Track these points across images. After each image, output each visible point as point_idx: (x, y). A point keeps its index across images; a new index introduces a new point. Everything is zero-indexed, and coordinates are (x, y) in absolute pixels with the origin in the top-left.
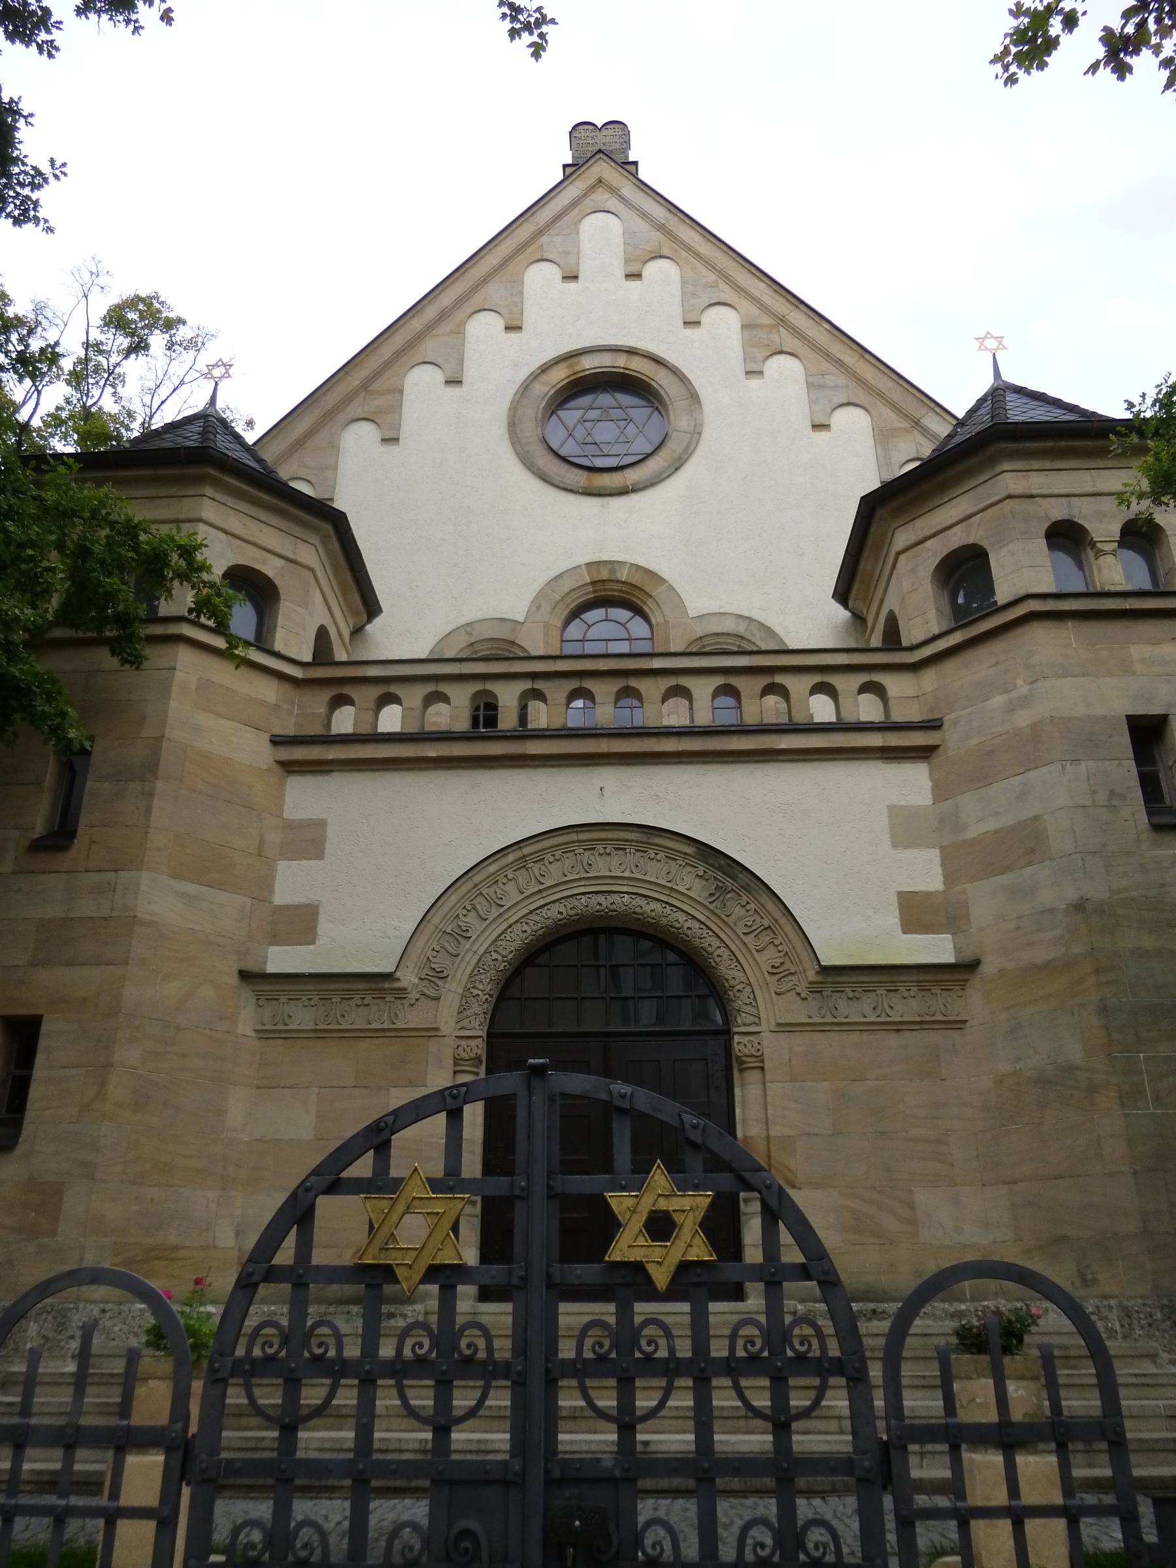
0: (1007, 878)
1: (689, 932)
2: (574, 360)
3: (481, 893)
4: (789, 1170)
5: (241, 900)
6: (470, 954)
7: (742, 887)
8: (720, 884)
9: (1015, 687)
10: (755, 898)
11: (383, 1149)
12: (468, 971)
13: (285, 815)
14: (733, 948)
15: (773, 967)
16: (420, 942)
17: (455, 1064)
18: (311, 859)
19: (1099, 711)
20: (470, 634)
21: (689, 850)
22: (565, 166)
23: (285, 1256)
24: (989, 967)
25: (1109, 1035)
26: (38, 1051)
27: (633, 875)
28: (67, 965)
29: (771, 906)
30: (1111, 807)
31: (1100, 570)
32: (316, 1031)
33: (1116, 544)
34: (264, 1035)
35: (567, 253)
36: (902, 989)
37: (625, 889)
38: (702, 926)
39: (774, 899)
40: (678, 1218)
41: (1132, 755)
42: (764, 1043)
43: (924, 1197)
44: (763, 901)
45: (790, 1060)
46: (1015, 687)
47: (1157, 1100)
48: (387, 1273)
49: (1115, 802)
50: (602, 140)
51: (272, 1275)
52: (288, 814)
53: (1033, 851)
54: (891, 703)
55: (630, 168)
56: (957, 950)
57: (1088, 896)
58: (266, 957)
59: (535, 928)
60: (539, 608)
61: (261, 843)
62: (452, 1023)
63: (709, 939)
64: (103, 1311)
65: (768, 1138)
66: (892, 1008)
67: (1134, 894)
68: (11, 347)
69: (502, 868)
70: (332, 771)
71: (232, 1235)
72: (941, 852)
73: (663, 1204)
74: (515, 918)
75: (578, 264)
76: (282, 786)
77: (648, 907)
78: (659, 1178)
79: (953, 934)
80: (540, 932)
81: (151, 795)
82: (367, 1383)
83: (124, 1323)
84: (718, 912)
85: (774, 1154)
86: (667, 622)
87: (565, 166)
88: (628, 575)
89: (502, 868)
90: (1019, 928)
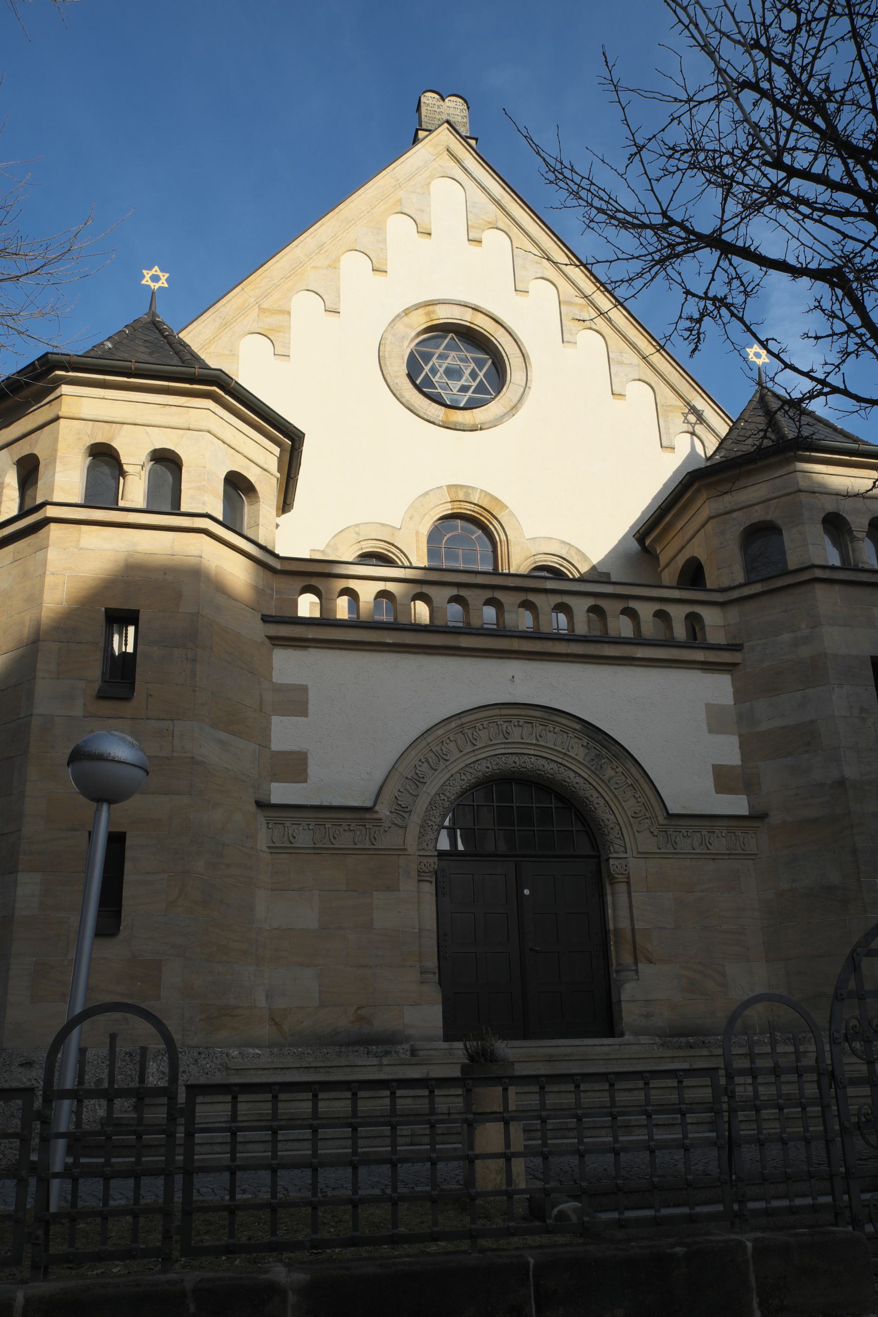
2: (431, 308)
3: (431, 750)
7: (613, 755)
8: (598, 753)
10: (623, 764)
13: (274, 680)
14: (607, 798)
15: (635, 813)
17: (419, 875)
18: (298, 716)
20: (358, 534)
21: (577, 727)
26: (126, 860)
27: (538, 743)
29: (633, 770)
32: (314, 848)
33: (865, 534)
34: (273, 849)
35: (422, 211)
36: (717, 831)
37: (532, 752)
38: (585, 782)
39: (636, 765)
41: (873, 684)
44: (628, 767)
45: (647, 877)
56: (751, 806)
58: (270, 791)
60: (411, 518)
63: (590, 791)
64: (200, 1053)
65: (633, 930)
66: (711, 844)
69: (446, 732)
70: (309, 647)
72: (740, 738)
74: (456, 769)
75: (430, 223)
77: (550, 767)
79: (747, 795)
80: (473, 781)
83: (212, 1062)
84: (597, 772)
88: (479, 498)
89: (446, 732)
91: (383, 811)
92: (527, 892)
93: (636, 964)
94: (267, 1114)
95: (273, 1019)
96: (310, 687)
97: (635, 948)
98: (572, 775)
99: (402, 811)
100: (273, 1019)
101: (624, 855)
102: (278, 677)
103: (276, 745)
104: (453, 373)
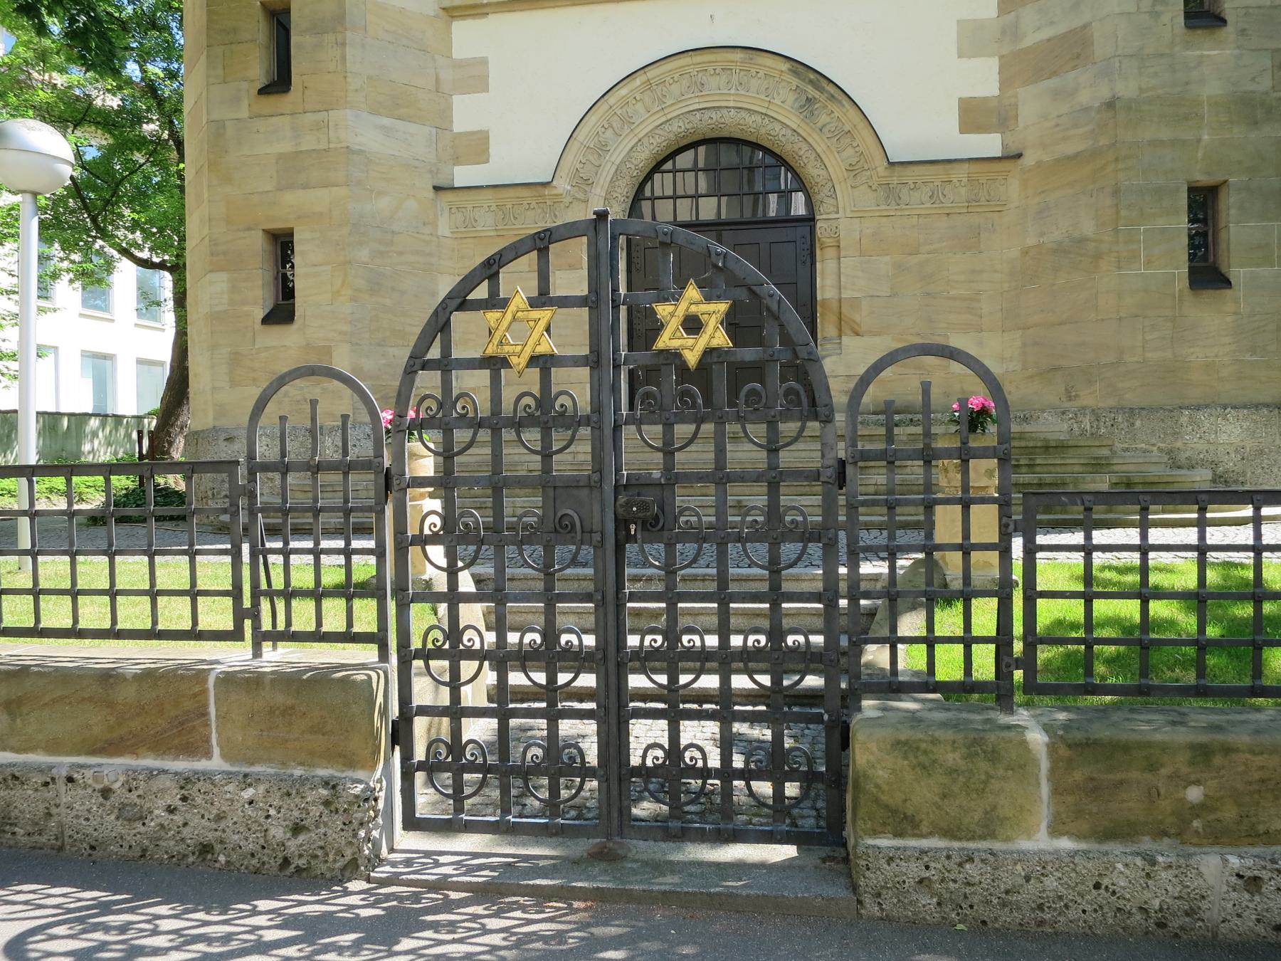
0: (1053, 82)
1: (783, 139)
4: (854, 322)
6: (609, 164)
11: (493, 277)
16: (569, 156)
23: (434, 353)
24: (1029, 160)
25: (1118, 213)
28: (304, 188)
37: (731, 104)
40: (704, 318)
42: (840, 227)
47: (1149, 263)
48: (503, 362)
51: (426, 366)
52: (457, 54)
53: (1078, 56)
57: (1120, 95)
59: (659, 141)
61: (437, 81)
65: (840, 300)
67: (1160, 92)
73: (693, 309)
74: (644, 133)
76: (449, 25)
77: (751, 120)
79: (1003, 133)
80: (665, 144)
81: (344, 44)
82: (496, 431)
85: (844, 310)
90: (1057, 125)
93: (840, 336)
96: (490, 59)
97: (840, 319)
98: (778, 127)
101: (836, 216)
103: (458, 127)
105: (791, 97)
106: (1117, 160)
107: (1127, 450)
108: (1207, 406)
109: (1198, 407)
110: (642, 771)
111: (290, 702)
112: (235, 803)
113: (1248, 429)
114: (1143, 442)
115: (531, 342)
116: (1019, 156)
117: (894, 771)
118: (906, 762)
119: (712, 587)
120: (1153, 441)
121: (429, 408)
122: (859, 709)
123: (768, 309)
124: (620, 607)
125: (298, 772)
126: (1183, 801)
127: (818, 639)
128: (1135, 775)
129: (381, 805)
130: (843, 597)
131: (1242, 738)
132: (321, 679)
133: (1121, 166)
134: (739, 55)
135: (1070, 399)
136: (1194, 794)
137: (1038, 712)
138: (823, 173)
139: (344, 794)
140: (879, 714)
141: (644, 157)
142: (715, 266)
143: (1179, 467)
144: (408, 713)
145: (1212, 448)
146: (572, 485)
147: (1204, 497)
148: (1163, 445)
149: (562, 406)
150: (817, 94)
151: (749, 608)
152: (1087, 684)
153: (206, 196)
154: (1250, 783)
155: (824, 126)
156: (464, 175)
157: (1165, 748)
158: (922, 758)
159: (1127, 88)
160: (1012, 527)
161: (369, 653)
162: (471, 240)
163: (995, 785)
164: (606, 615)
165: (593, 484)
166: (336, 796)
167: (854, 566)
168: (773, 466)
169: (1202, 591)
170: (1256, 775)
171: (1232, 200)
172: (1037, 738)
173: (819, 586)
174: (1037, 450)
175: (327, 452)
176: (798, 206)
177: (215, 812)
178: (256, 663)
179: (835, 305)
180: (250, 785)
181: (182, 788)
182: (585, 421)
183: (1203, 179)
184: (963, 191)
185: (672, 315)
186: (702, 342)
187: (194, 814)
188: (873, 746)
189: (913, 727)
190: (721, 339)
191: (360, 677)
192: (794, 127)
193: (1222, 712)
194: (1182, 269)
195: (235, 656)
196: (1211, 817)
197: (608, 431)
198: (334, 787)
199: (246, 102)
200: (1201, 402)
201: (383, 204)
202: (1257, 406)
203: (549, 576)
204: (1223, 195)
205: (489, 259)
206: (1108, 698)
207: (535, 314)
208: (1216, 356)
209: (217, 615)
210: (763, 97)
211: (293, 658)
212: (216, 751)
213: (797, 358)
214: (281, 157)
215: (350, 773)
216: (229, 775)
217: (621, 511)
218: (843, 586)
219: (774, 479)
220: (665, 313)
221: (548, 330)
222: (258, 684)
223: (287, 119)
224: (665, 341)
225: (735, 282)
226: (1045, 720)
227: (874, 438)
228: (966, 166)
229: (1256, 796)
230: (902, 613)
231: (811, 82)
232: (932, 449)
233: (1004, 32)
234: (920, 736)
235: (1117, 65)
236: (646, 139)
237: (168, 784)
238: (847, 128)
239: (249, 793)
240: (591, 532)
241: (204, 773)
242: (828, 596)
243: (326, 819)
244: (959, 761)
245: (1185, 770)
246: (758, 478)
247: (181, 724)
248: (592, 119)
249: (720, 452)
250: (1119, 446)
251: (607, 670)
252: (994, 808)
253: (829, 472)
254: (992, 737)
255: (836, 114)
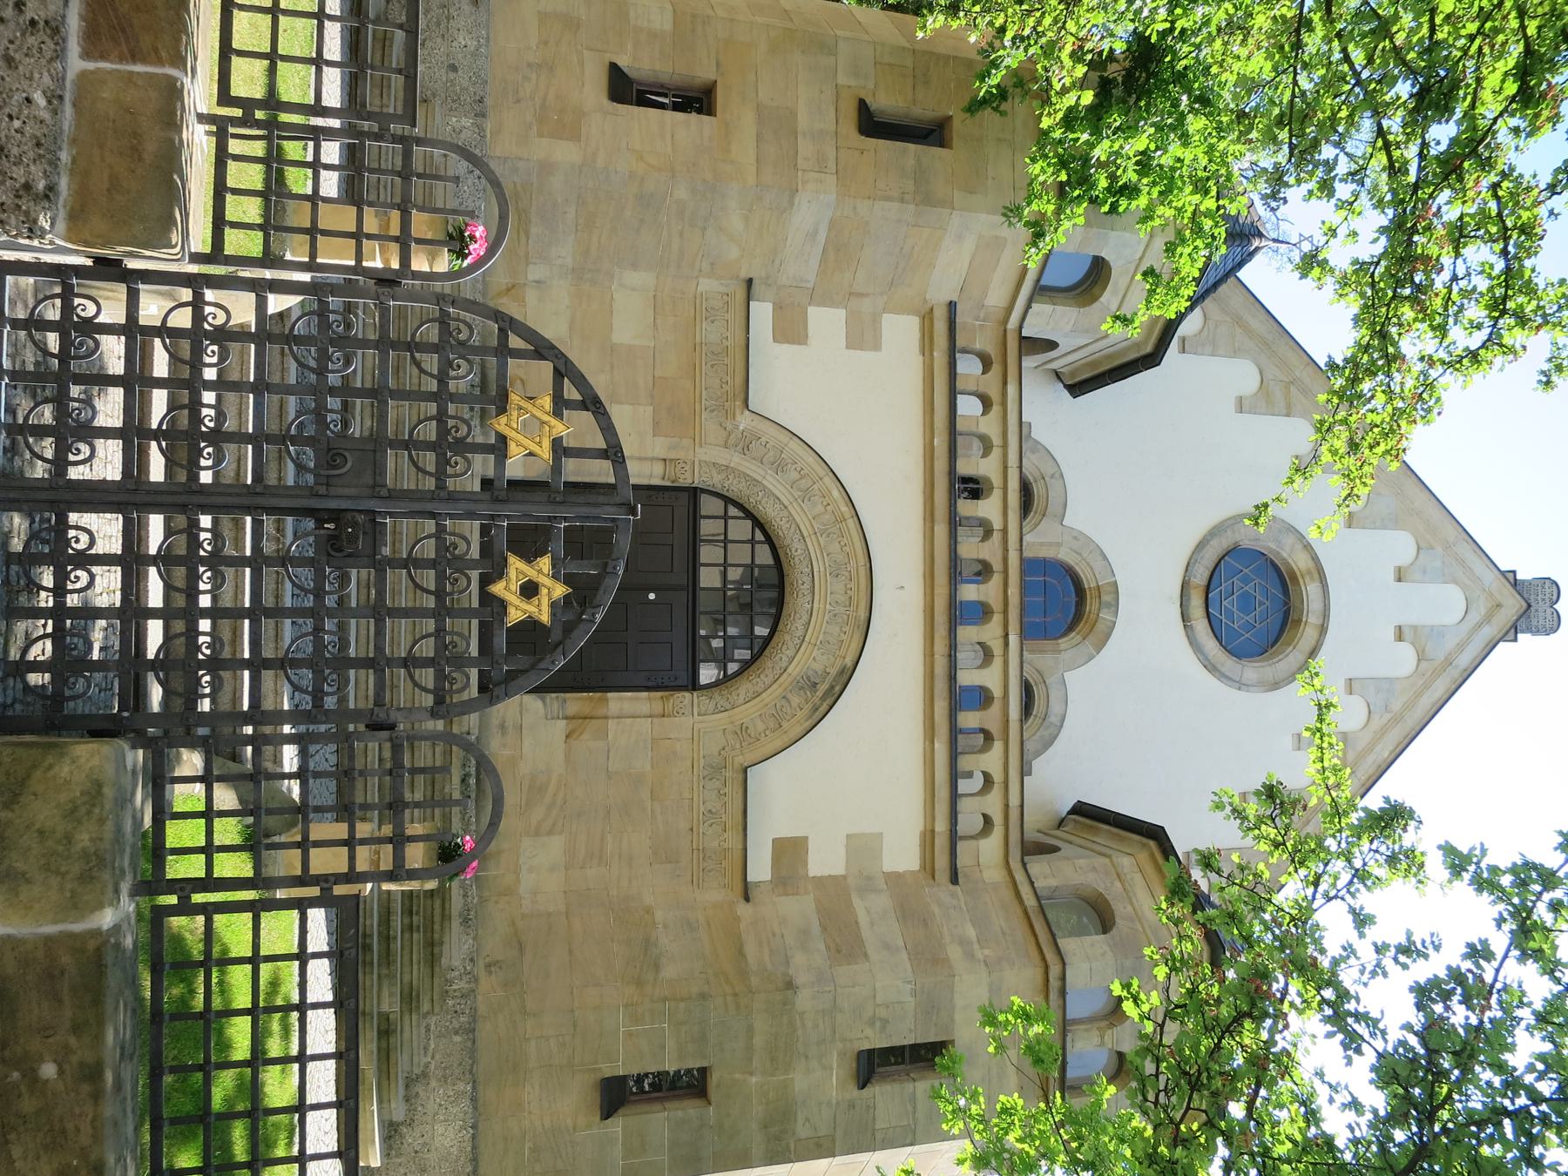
0: (816, 929)
2: (1316, 576)
5: (811, 278)
6: (762, 473)
9: (982, 948)
11: (583, 406)
12: (748, 472)
13: (885, 316)
16: (772, 431)
17: (671, 460)
19: (958, 1017)
20: (1052, 476)
22: (1514, 572)
23: (515, 342)
24: (743, 909)
25: (682, 1000)
30: (871, 1023)
31: (1086, 1030)
35: (1425, 572)
37: (816, 605)
40: (535, 600)
42: (683, 718)
43: (556, 844)
46: (982, 948)
47: (630, 1034)
49: (878, 1024)
50: (1540, 607)
53: (839, 951)
54: (973, 843)
55: (1512, 632)
60: (1075, 538)
61: (861, 295)
62: (707, 458)
65: (606, 718)
67: (800, 1032)
68: (1127, 147)
71: (537, 277)
73: (544, 591)
74: (793, 512)
77: (799, 625)
78: (560, 590)
81: (902, 201)
85: (594, 721)
86: (1059, 652)
87: (1514, 572)
90: (774, 935)
91: (744, 421)
92: (652, 596)
94: (405, 385)
95: (513, 286)
98: (790, 653)
99: (746, 444)
100: (513, 286)
102: (888, 320)
103: (813, 311)
104: (1246, 603)
105: (818, 667)
106: (735, 995)
107: (428, 1029)
108: (475, 1108)
109: (474, 1100)
110: (63, 525)
111: (148, 157)
112: (28, 82)
113: (449, 1154)
114: (437, 1045)
115: (520, 437)
116: (747, 899)
117: (67, 782)
118: (78, 794)
119: (268, 601)
120: (437, 1057)
121: (460, 332)
122: (134, 747)
123: (541, 660)
124: (248, 510)
125: (65, 156)
126: (41, 1060)
127: (205, 705)
128: (68, 1013)
129: (22, 241)
130: (254, 730)
131: (109, 1110)
132: (171, 194)
133: (729, 999)
134: (863, 614)
135: (488, 966)
136: (49, 1070)
137: (133, 921)
138: (741, 701)
139: (38, 208)
140: (129, 767)
141: (769, 511)
142: (582, 613)
143: (407, 1086)
144: (132, 279)
145: (429, 1119)
146: (378, 469)
147: (352, 1056)
148: (432, 1066)
149: (456, 463)
150: (820, 694)
151: (242, 634)
152: (164, 964)
153: (759, 20)
154: (61, 1120)
155: (788, 701)
156: (762, 312)
157: (99, 1038)
158: (83, 810)
159: (804, 1000)
160: (325, 885)
161: (201, 239)
162: (692, 313)
163: (54, 881)
164: (238, 495)
165: (376, 488)
166: (37, 198)
167: (290, 739)
168: (390, 662)
169: (260, 1113)
170: (70, 1126)
171: (691, 1111)
172: (106, 918)
173: (268, 704)
174: (429, 935)
175: (454, 119)
176: (707, 674)
177: (17, 56)
178: (192, 118)
179: (601, 712)
180: (49, 102)
181: (47, 22)
182: (441, 486)
183: (714, 1080)
184: (715, 844)
185: (540, 571)
186: (513, 598)
187: (14, 32)
188: (95, 761)
189: (116, 799)
190: (514, 616)
191: (175, 237)
192: (789, 670)
193: (134, 1096)
194: (621, 1067)
195: (200, 94)
196: (23, 1088)
197: (429, 507)
198: (47, 197)
199: (853, 83)
200: (481, 1102)
201: (735, 222)
202: (475, 1160)
203: (282, 439)
204: (698, 1102)
205: (601, 402)
206: (148, 994)
207: (547, 444)
208: (530, 1113)
209: (248, 80)
210: (821, 638)
211: (198, 157)
212: (91, 66)
213: (495, 686)
214: (793, 114)
215: (62, 214)
216: (60, 80)
217: (349, 516)
218: (268, 730)
219: (376, 663)
220: (541, 565)
221: (531, 454)
222: (168, 124)
223: (833, 128)
224: (515, 564)
225: (568, 629)
226: (125, 927)
227: (448, 757)
228: (740, 846)
229: (47, 1128)
230: (236, 789)
231: (832, 687)
232: (403, 811)
233: (869, 878)
234: (107, 807)
235: (827, 989)
236: (786, 514)
237: (52, 8)
238: (785, 724)
239: (39, 99)
240: (328, 485)
241: (64, 50)
242: (257, 714)
243: (8, 184)
244: (80, 845)
245: (75, 1059)
246: (379, 648)
247: (123, 30)
248: (811, 459)
249: (406, 613)
250: (433, 1020)
251: (181, 493)
252: (28, 881)
253: (382, 716)
254: (106, 876)
255: (799, 713)
